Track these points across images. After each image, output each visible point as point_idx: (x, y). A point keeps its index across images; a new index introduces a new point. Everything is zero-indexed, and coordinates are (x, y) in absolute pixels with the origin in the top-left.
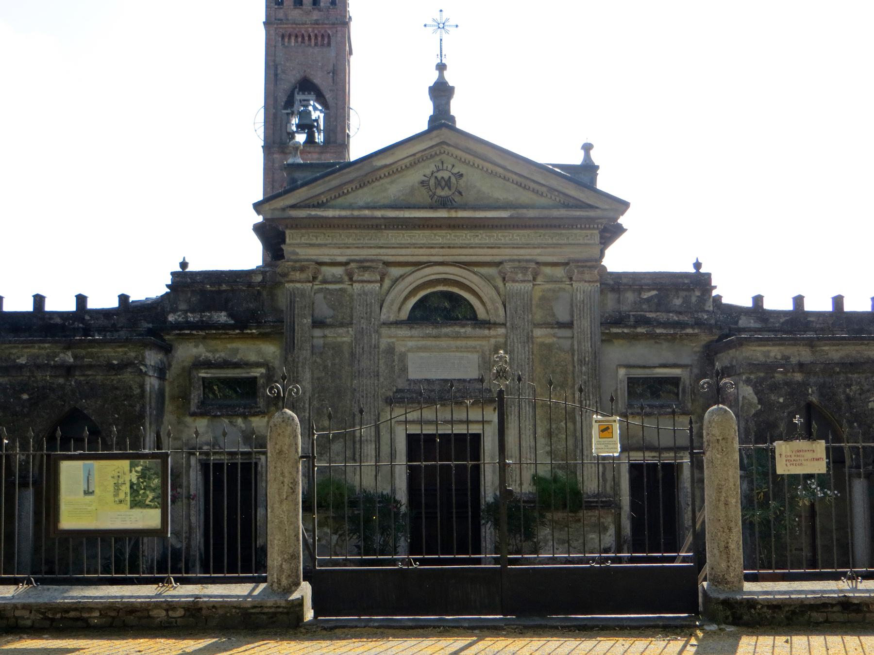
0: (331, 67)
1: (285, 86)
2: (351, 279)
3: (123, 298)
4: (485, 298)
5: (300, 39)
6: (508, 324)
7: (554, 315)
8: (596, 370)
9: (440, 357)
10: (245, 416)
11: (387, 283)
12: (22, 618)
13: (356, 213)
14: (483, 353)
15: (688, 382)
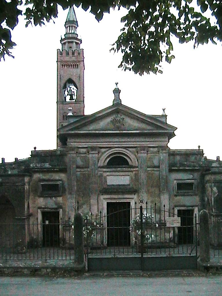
0: (78, 76)
1: (63, 82)
2: (88, 153)
3: (16, 159)
4: (132, 158)
5: (68, 66)
6: (139, 167)
7: (153, 164)
8: (167, 182)
9: (118, 179)
10: (55, 197)
11: (100, 155)
12: (5, 271)
13: (90, 132)
14: (131, 176)
15: (196, 184)
